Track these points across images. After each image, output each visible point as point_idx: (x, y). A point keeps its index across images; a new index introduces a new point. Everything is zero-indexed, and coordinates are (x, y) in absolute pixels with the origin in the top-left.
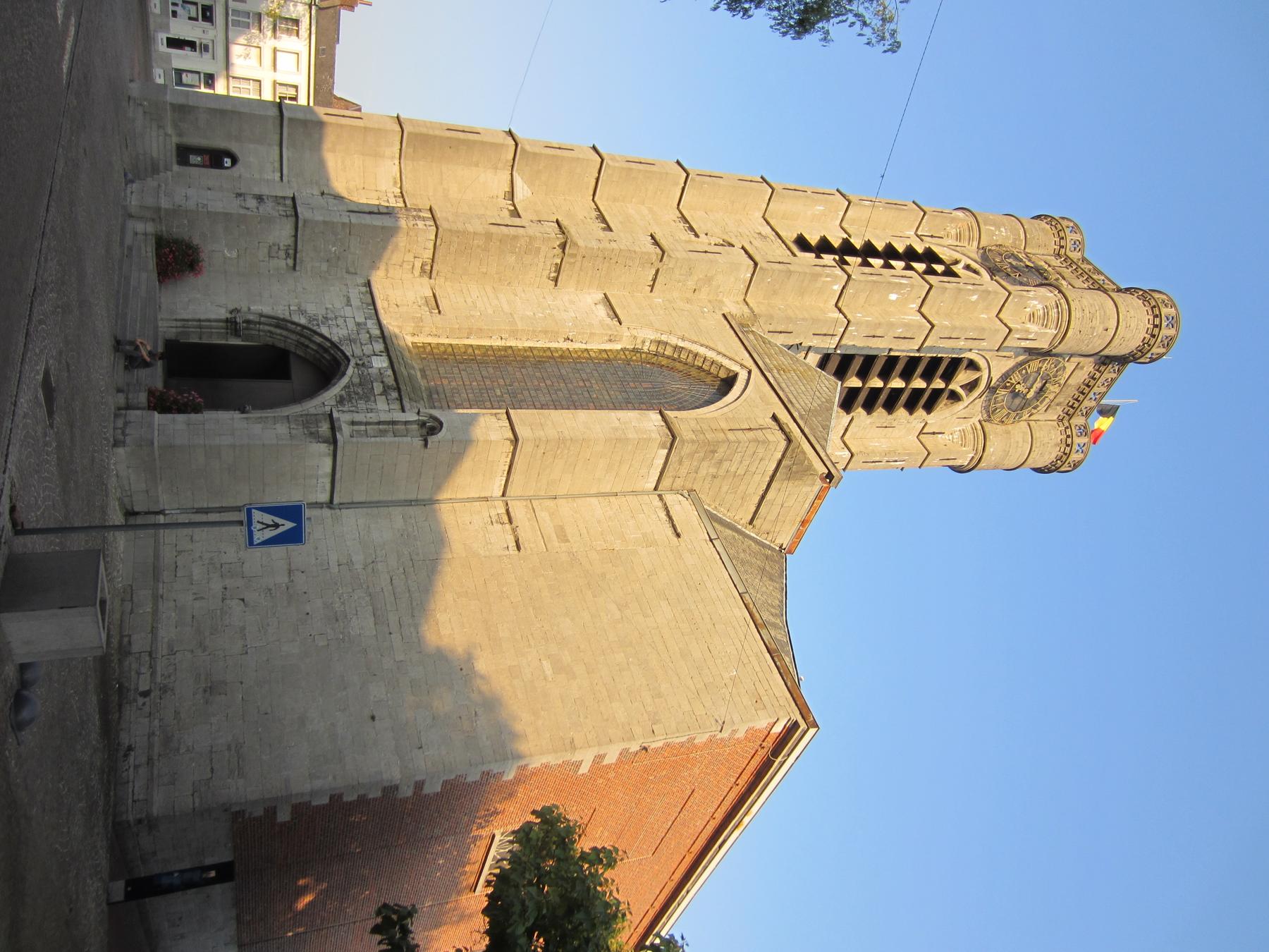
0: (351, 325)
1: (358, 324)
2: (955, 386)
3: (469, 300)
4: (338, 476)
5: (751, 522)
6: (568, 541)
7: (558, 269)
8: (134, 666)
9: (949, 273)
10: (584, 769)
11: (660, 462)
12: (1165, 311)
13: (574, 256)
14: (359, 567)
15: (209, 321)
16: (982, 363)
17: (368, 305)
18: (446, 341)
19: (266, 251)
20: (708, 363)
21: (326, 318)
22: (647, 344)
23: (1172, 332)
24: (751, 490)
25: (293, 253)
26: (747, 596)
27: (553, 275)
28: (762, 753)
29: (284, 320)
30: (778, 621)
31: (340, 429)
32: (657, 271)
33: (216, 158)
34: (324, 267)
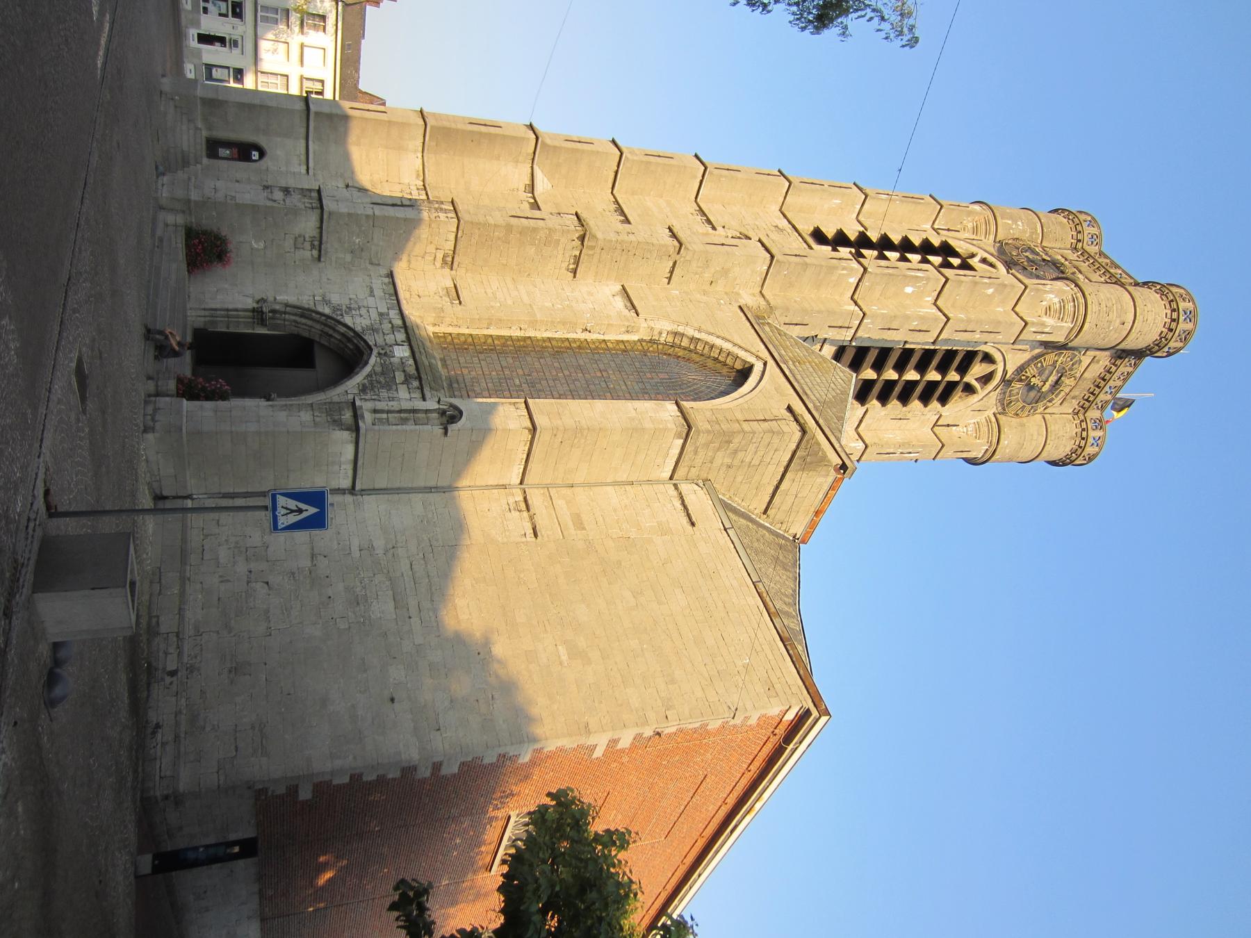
0: (374, 315)
1: (381, 314)
2: (970, 378)
3: (489, 291)
4: (360, 463)
5: (765, 512)
6: (584, 529)
7: (577, 261)
8: (162, 646)
9: (965, 266)
10: (598, 753)
11: (675, 452)
12: (1182, 305)
13: (593, 248)
14: (380, 552)
15: (237, 310)
16: (997, 356)
17: (390, 295)
18: (467, 331)
19: (292, 242)
20: (724, 355)
21: (350, 308)
22: (664, 335)
23: (1189, 326)
24: (765, 481)
25: (318, 245)
26: (760, 585)
27: (572, 266)
28: (774, 740)
29: (309, 310)
30: (791, 610)
31: (363, 417)
32: (675, 263)
33: (245, 151)
34: (348, 258)
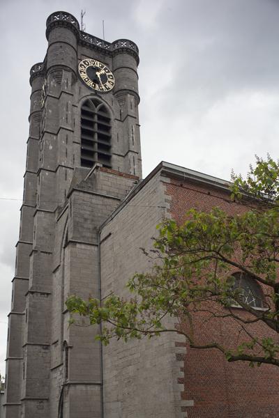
2: (96, 110)
4: (86, 382)
11: (83, 246)
16: (84, 100)
19: (40, 411)
25: (41, 400)
27: (46, 295)
32: (42, 252)
34: (46, 388)
